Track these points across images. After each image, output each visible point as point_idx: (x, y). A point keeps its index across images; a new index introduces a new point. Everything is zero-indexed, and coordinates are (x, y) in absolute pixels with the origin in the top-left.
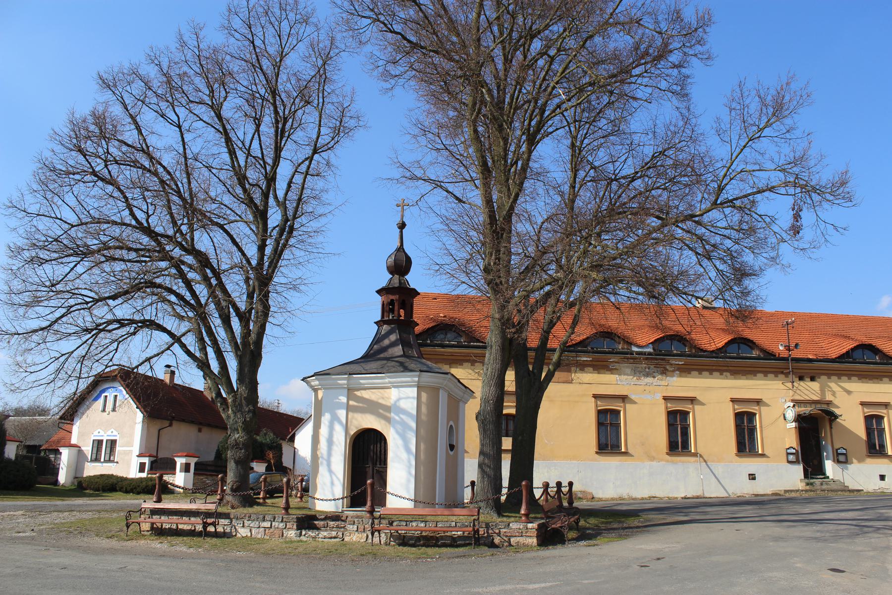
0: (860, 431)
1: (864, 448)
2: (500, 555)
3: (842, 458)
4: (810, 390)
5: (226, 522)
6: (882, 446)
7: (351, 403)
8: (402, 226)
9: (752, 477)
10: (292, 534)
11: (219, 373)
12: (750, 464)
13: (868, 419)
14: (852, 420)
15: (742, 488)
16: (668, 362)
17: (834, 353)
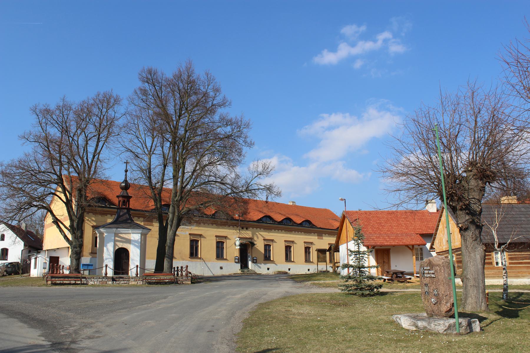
0: (262, 250)
1: (263, 258)
2: (178, 286)
3: (255, 261)
4: (247, 234)
5: (84, 280)
6: (270, 257)
7: (117, 238)
8: (126, 171)
9: (221, 268)
10: (110, 283)
11: (70, 226)
12: (221, 263)
13: (266, 246)
14: (260, 246)
15: (218, 273)
16: (192, 219)
17: (256, 218)
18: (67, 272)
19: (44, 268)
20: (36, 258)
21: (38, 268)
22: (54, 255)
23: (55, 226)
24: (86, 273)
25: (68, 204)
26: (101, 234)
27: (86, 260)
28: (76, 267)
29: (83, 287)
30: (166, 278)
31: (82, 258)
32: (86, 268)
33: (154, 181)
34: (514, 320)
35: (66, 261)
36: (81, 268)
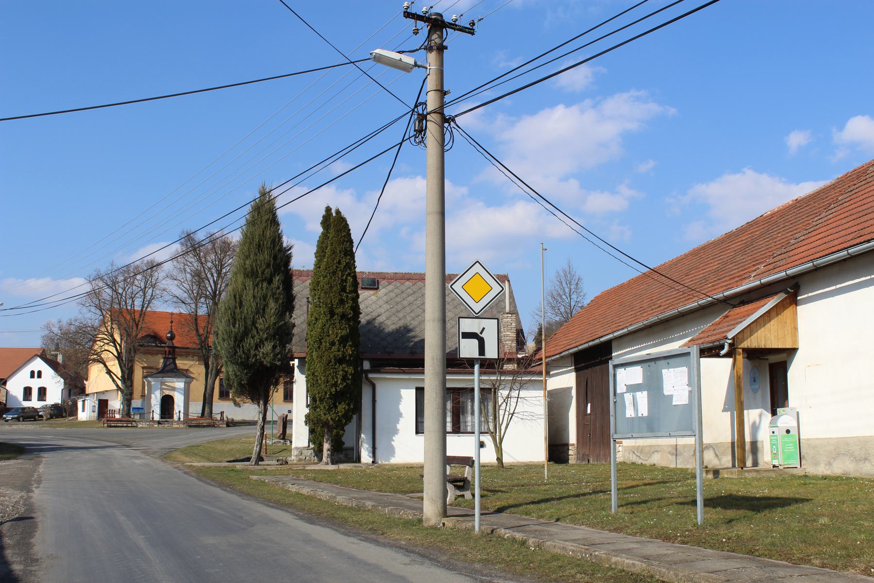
18: (118, 416)
19: (94, 412)
20: (84, 401)
21: (86, 412)
22: (103, 397)
23: (108, 376)
24: (137, 417)
26: (149, 382)
27: (136, 403)
28: (127, 411)
29: (133, 429)
30: (204, 422)
31: (133, 401)
33: (201, 331)
34: (561, 466)
35: (116, 404)
36: (132, 412)
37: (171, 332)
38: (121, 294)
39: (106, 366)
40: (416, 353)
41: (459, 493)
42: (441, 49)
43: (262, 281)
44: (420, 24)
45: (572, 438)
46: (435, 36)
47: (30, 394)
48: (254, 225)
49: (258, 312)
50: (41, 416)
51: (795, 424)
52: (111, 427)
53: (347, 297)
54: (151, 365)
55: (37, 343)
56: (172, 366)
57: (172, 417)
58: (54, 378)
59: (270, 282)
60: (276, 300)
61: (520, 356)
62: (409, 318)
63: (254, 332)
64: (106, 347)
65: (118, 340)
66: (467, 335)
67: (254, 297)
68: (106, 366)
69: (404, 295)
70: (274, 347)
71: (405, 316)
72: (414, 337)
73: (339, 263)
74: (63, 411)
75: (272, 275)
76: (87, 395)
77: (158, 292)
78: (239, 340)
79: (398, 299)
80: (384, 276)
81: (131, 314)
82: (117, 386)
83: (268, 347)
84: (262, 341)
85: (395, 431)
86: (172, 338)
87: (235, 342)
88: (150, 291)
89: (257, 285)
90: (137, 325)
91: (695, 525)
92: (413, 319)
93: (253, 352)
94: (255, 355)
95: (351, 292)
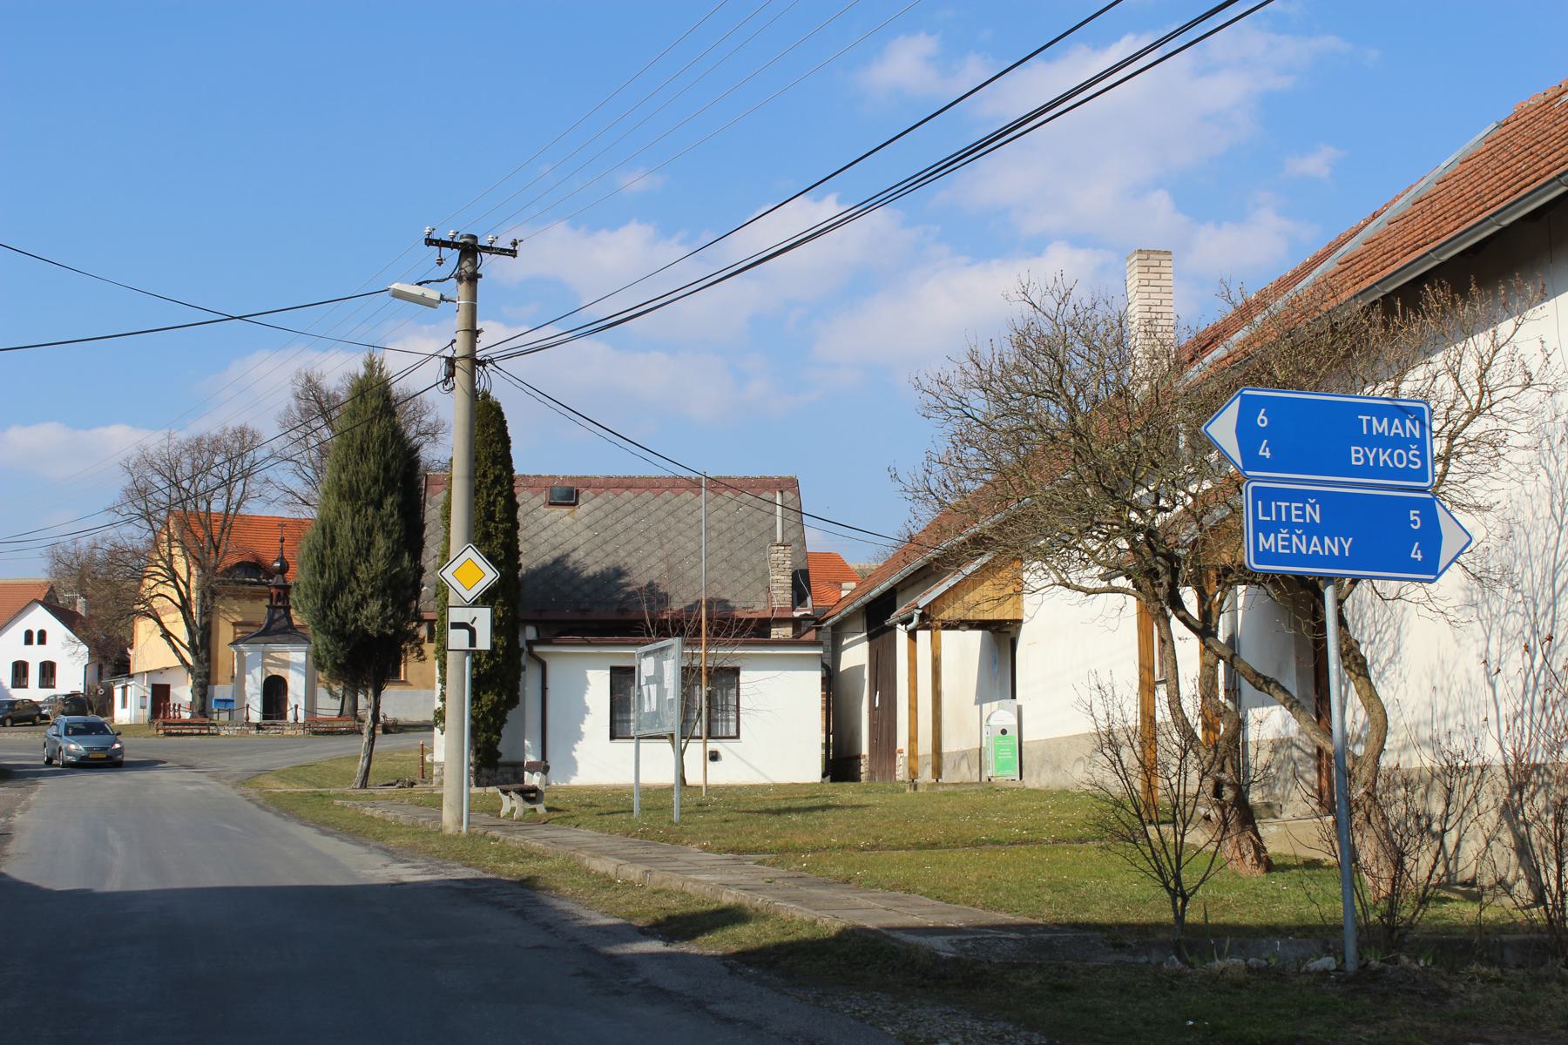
18: (186, 716)
19: (143, 707)
20: (124, 688)
21: (129, 708)
23: (164, 641)
25: (185, 607)
26: (240, 653)
27: (222, 690)
28: (203, 705)
32: (222, 705)
35: (183, 693)
37: (281, 559)
38: (188, 491)
39: (160, 623)
40: (626, 610)
41: (529, 806)
42: (473, 279)
43: (367, 505)
44: (446, 251)
45: (865, 750)
46: (465, 264)
47: (25, 674)
48: (354, 418)
49: (358, 554)
50: (46, 717)
51: (1015, 722)
52: (171, 734)
53: (496, 528)
54: (249, 619)
55: (37, 571)
56: (284, 622)
57: (284, 716)
58: (65, 646)
59: (379, 506)
60: (389, 534)
61: (796, 614)
62: (622, 553)
63: (354, 584)
64: (161, 589)
65: (183, 574)
66: (456, 626)
67: (353, 530)
68: (160, 623)
69: (619, 514)
70: (384, 607)
71: (616, 550)
72: (628, 585)
73: (484, 475)
74: (87, 709)
75: (383, 496)
76: (131, 677)
77: (253, 486)
78: (329, 597)
79: (608, 521)
80: (588, 483)
81: (205, 527)
82: (183, 660)
83: (374, 607)
84: (364, 598)
85: (579, 736)
86: (284, 569)
87: (323, 600)
88: (240, 485)
89: (359, 511)
90: (217, 548)
91: (671, 822)
92: (630, 554)
93: (351, 616)
94: (355, 620)
95: (502, 520)
